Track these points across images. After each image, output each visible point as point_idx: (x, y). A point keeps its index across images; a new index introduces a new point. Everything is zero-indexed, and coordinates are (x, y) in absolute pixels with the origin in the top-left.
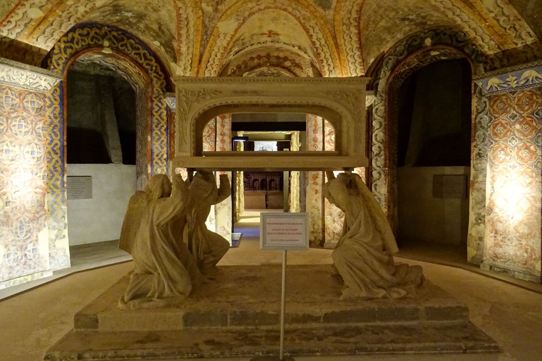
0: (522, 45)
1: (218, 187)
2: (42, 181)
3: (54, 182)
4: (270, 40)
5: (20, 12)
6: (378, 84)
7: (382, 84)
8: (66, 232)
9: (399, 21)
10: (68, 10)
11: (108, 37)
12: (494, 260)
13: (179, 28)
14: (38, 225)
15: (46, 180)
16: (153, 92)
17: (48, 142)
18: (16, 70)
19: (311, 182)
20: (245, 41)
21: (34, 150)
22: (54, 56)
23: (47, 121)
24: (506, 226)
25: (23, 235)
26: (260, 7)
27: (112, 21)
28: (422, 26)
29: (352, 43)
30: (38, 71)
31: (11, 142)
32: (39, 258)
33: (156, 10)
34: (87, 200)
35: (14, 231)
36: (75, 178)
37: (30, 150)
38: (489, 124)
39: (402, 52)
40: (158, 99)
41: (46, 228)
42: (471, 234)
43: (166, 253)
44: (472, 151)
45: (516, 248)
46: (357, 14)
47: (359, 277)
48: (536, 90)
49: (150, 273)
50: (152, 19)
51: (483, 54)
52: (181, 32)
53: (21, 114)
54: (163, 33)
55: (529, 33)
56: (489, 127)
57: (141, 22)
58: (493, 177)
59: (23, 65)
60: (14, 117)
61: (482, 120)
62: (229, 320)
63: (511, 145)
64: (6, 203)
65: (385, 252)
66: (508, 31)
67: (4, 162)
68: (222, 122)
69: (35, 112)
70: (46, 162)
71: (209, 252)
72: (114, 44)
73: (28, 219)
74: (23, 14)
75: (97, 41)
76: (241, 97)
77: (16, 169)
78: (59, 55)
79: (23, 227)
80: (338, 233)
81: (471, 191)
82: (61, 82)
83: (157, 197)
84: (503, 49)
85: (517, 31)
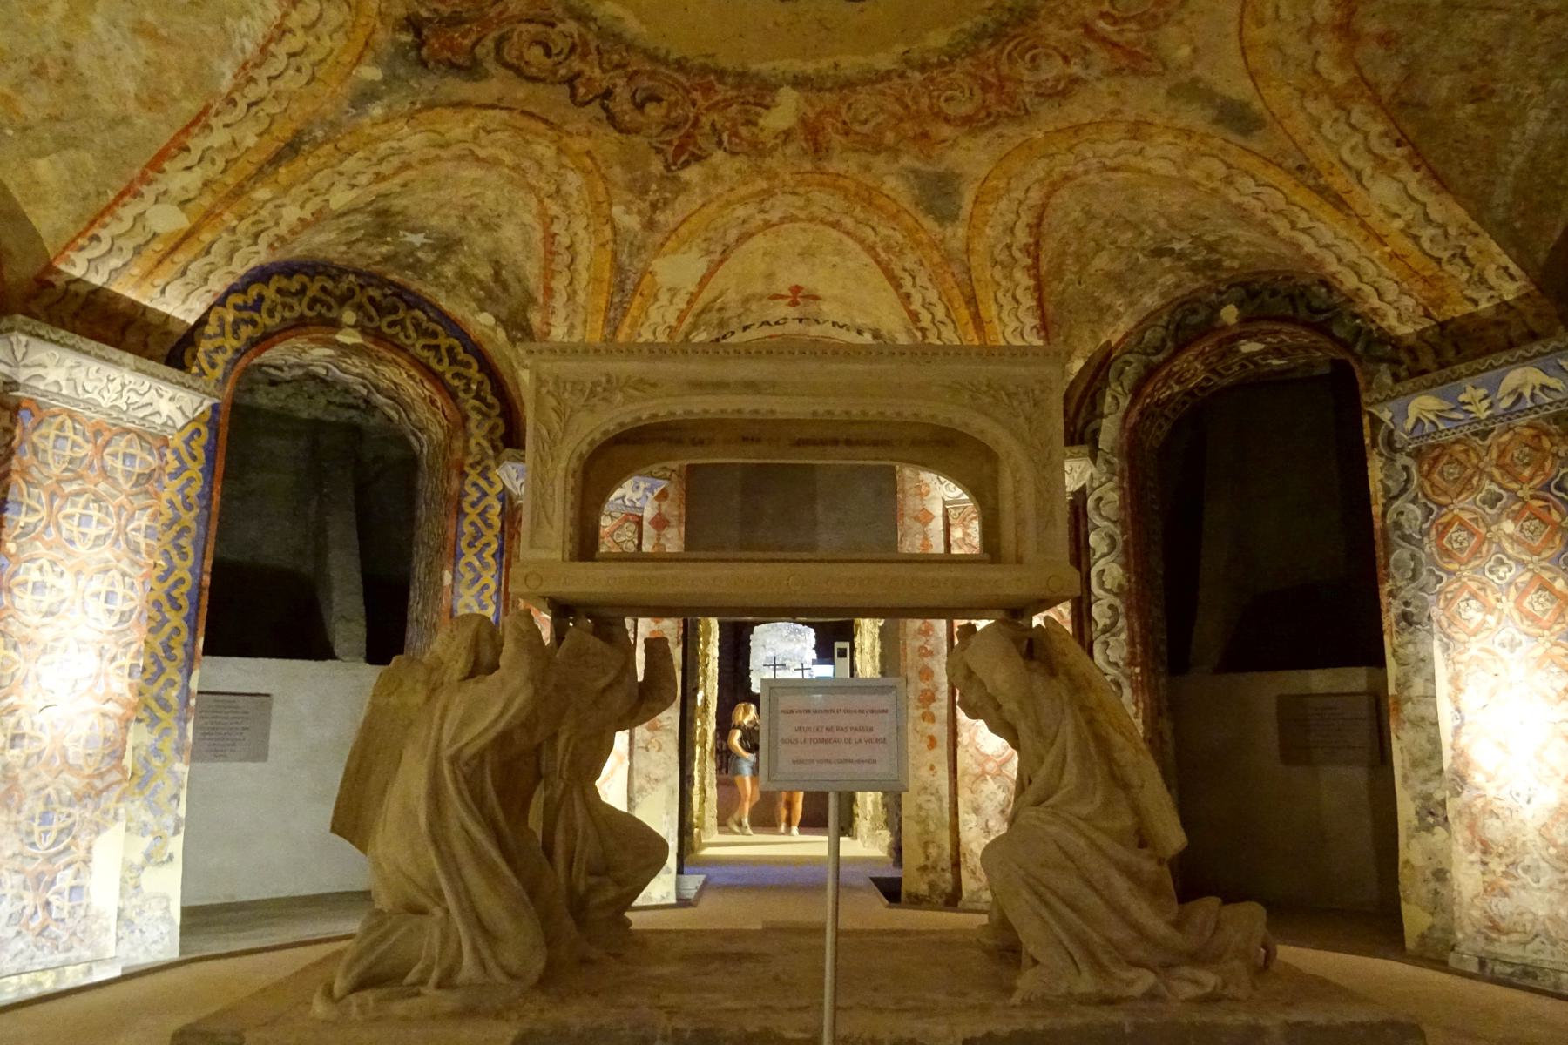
0: (1490, 304)
1: (640, 678)
2: (127, 680)
3: (161, 689)
4: (797, 316)
5: (128, 213)
6: (1096, 432)
7: (1109, 430)
8: (176, 845)
9: (1145, 256)
10: (255, 213)
11: (356, 299)
12: (1487, 938)
13: (548, 274)
14: (98, 813)
15: (138, 679)
16: (466, 451)
17: (158, 572)
18: (94, 366)
19: (914, 712)
20: (726, 315)
21: (116, 590)
23: (161, 514)
24: (1514, 828)
25: (50, 841)
26: (767, 216)
27: (370, 258)
28: (1210, 273)
29: (1020, 314)
31: (53, 563)
32: (85, 916)
33: (488, 226)
34: (251, 766)
35: (24, 827)
36: (221, 697)
37: (104, 589)
38: (1425, 526)
39: (1158, 344)
40: (479, 468)
41: (120, 827)
42: (1407, 862)
44: (1384, 608)
45: (1554, 896)
46: (1030, 235)
47: (1068, 929)
48: (1548, 423)
49: (422, 911)
50: (478, 251)
51: (1386, 338)
52: (554, 284)
53: (92, 487)
54: (505, 288)
55: (1506, 269)
56: (1427, 533)
57: (447, 260)
58: (1454, 680)
59: (116, 354)
61: (1403, 519)
63: (1497, 581)
64: (14, 737)
65: (1146, 851)
66: (1448, 268)
67: (24, 618)
68: (659, 539)
69: (131, 484)
70: (145, 628)
71: (603, 870)
72: (371, 319)
73: (69, 793)
74: (135, 219)
75: (324, 311)
76: (710, 399)
77: (57, 639)
78: (218, 342)
79: (50, 816)
81: (1393, 727)
82: (214, 408)
83: (457, 676)
84: (1440, 319)
85: (1472, 266)
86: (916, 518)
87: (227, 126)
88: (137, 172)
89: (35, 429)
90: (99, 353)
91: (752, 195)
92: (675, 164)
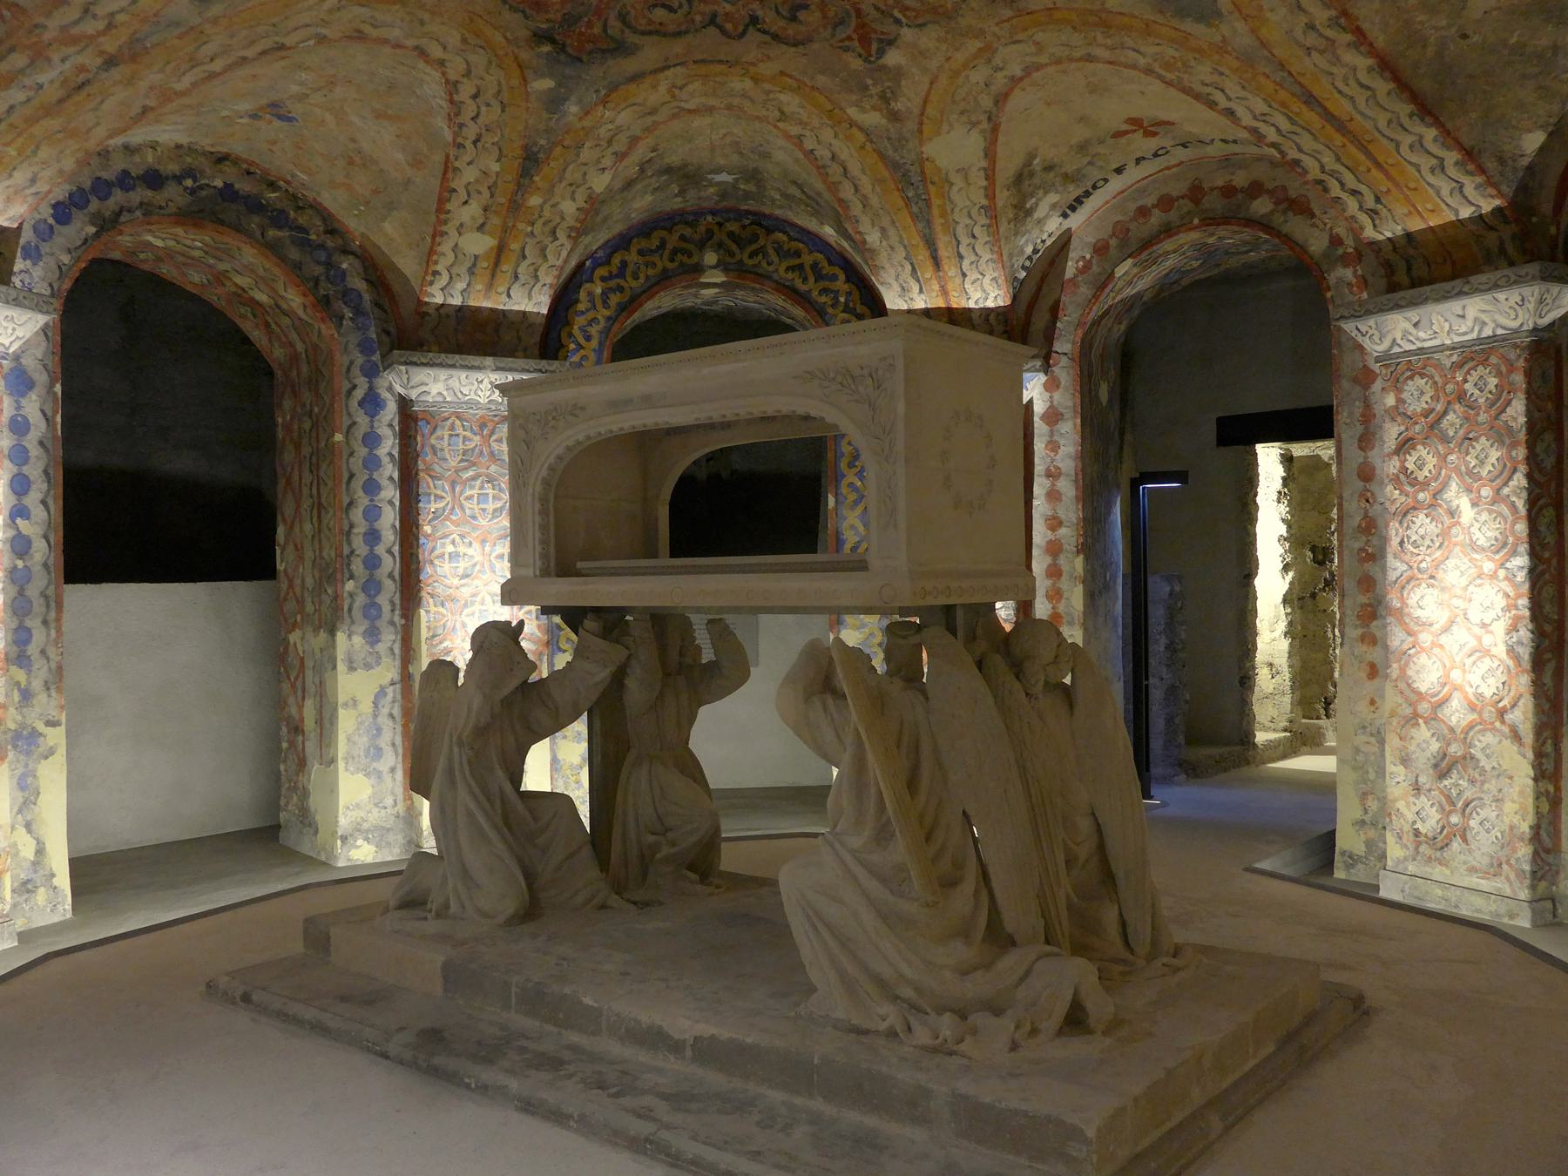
5: (446, 247)
18: (463, 374)
22: (577, 318)
30: (515, 366)
31: (462, 536)
43: (470, 814)
60: (468, 479)
62: (514, 1000)
72: (732, 255)
75: (685, 259)
77: (474, 595)
78: (590, 315)
80: (1430, 835)
86: (1355, 380)
87: (469, 163)
88: (433, 219)
89: (432, 434)
90: (463, 363)
91: (975, 56)
92: (871, 56)
